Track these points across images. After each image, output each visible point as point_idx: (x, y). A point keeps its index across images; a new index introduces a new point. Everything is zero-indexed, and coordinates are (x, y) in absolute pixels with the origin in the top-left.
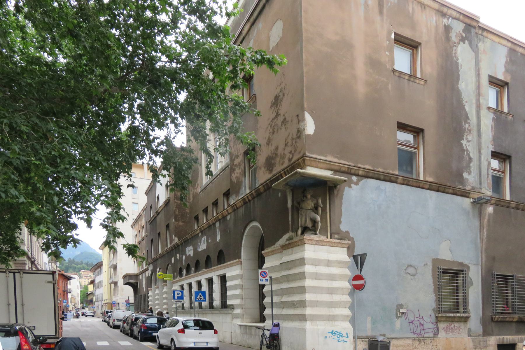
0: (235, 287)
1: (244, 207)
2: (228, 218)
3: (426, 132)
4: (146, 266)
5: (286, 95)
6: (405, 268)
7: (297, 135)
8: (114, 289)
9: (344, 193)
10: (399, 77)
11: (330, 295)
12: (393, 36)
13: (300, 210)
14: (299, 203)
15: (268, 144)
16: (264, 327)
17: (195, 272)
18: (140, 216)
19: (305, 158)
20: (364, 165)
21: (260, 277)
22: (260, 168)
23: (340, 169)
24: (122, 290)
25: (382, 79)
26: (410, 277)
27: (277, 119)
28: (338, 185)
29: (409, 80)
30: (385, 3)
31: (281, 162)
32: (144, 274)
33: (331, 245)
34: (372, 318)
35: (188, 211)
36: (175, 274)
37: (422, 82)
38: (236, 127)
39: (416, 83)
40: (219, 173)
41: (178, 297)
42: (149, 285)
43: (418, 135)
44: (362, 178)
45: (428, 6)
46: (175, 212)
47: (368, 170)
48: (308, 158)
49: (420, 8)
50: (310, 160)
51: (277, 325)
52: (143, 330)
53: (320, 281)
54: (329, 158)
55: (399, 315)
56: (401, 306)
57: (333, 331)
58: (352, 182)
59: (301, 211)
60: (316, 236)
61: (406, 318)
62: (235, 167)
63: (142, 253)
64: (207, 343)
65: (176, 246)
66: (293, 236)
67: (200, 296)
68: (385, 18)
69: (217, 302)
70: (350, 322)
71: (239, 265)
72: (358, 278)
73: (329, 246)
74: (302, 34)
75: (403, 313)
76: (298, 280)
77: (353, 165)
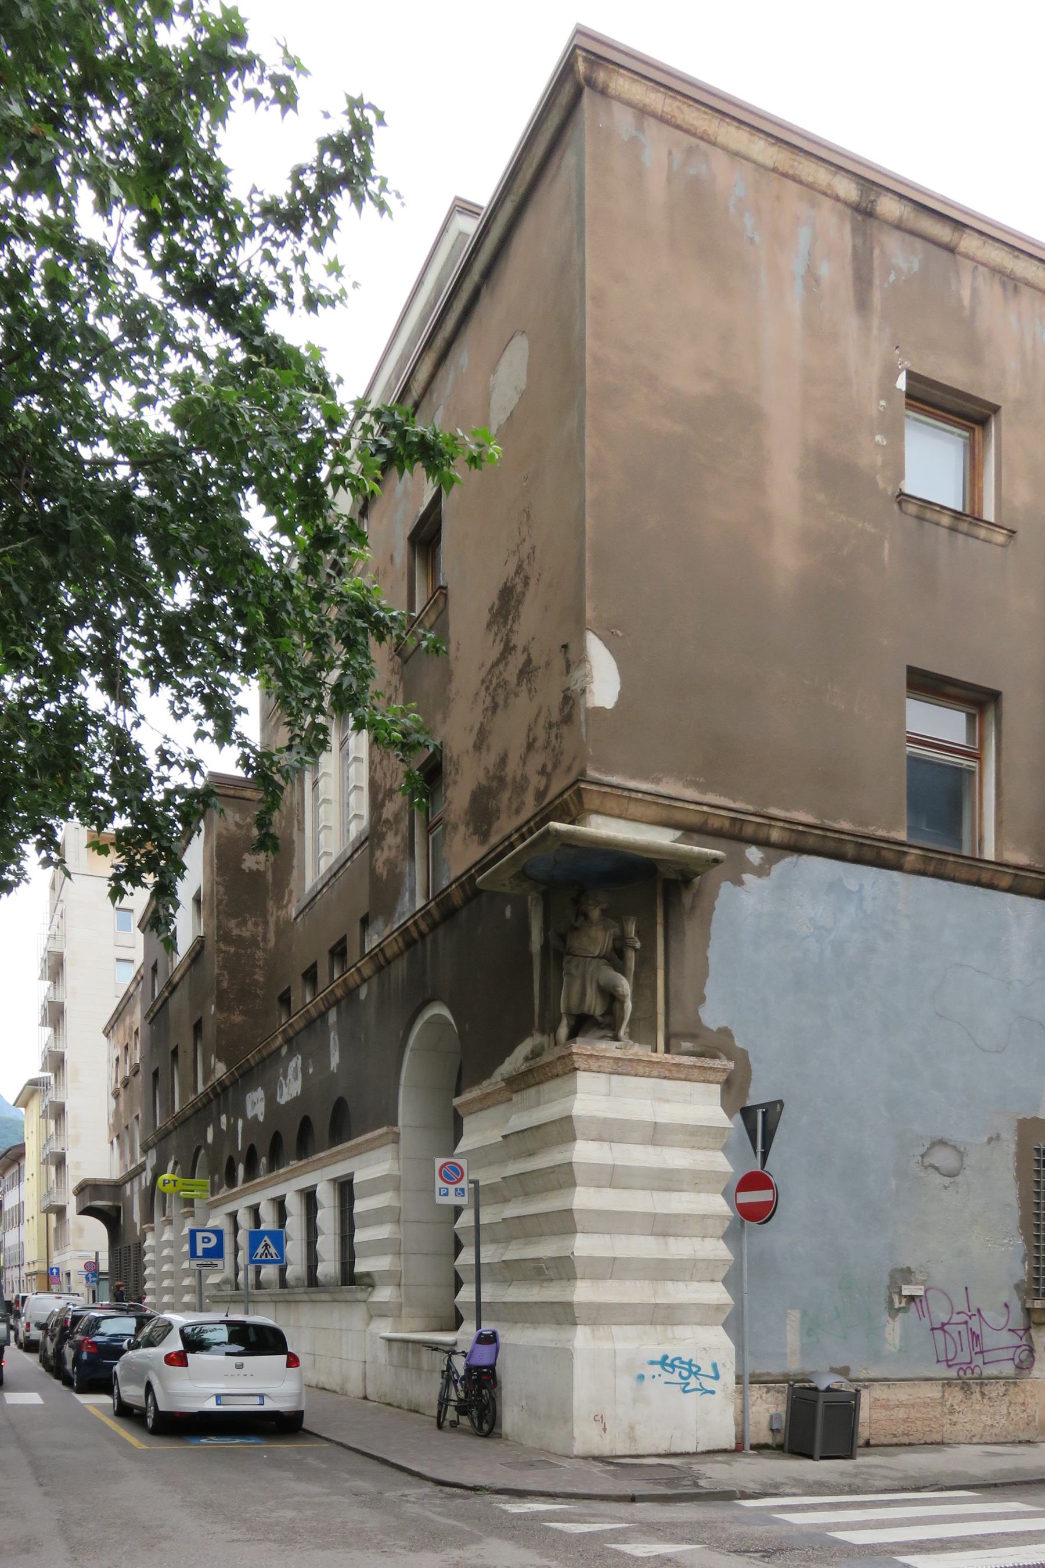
0: (376, 1217)
1: (406, 955)
2: (363, 993)
3: (1008, 705)
4: (142, 1156)
5: (532, 582)
6: (923, 1150)
7: (561, 710)
8: (56, 1229)
9: (717, 903)
10: (920, 518)
11: (661, 1239)
12: (901, 383)
13: (567, 958)
14: (563, 938)
15: (478, 747)
16: (455, 1344)
17: (271, 1168)
18: (127, 999)
19: (583, 786)
20: (787, 810)
21: (439, 1183)
22: (455, 828)
23: (706, 822)
24: (80, 1231)
25: (860, 525)
26: (938, 1179)
27: (506, 664)
28: (697, 875)
29: (953, 529)
30: (877, 273)
31: (514, 806)
32: (136, 1181)
33: (667, 1074)
34: (804, 1313)
35: (259, 977)
36: (217, 1177)
37: (1000, 537)
38: (351, 686)
39: (977, 538)
40: (349, 853)
41: (205, 1250)
42: (148, 1217)
43: (982, 712)
44: (780, 852)
45: (1028, 284)
46: (219, 983)
47: (800, 828)
48: (594, 787)
49: (997, 289)
50: (599, 792)
51: (489, 1340)
52: (85, 1356)
53: (625, 1194)
54: (668, 787)
55: (897, 1305)
56: (906, 1275)
57: (666, 1357)
58: (743, 865)
59: (569, 962)
60: (617, 1044)
61: (921, 1315)
62: (384, 830)
63: (131, 1114)
64: (261, 1396)
65: (219, 1090)
66: (543, 1047)
67: (266, 1245)
68: (876, 321)
69: (328, 1267)
70: (725, 1325)
71: (391, 1147)
72: (754, 1181)
73: (659, 1077)
74: (584, 373)
75: (912, 1298)
76: (553, 1189)
77: (750, 808)
